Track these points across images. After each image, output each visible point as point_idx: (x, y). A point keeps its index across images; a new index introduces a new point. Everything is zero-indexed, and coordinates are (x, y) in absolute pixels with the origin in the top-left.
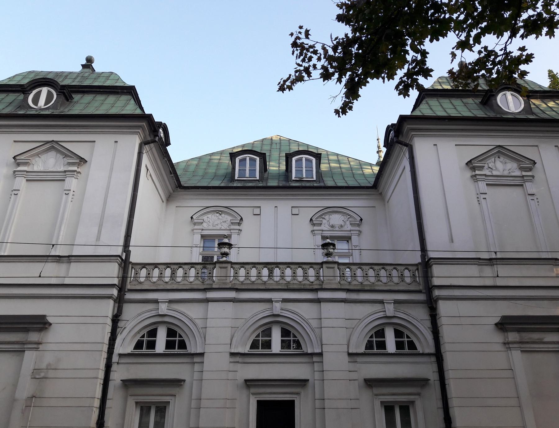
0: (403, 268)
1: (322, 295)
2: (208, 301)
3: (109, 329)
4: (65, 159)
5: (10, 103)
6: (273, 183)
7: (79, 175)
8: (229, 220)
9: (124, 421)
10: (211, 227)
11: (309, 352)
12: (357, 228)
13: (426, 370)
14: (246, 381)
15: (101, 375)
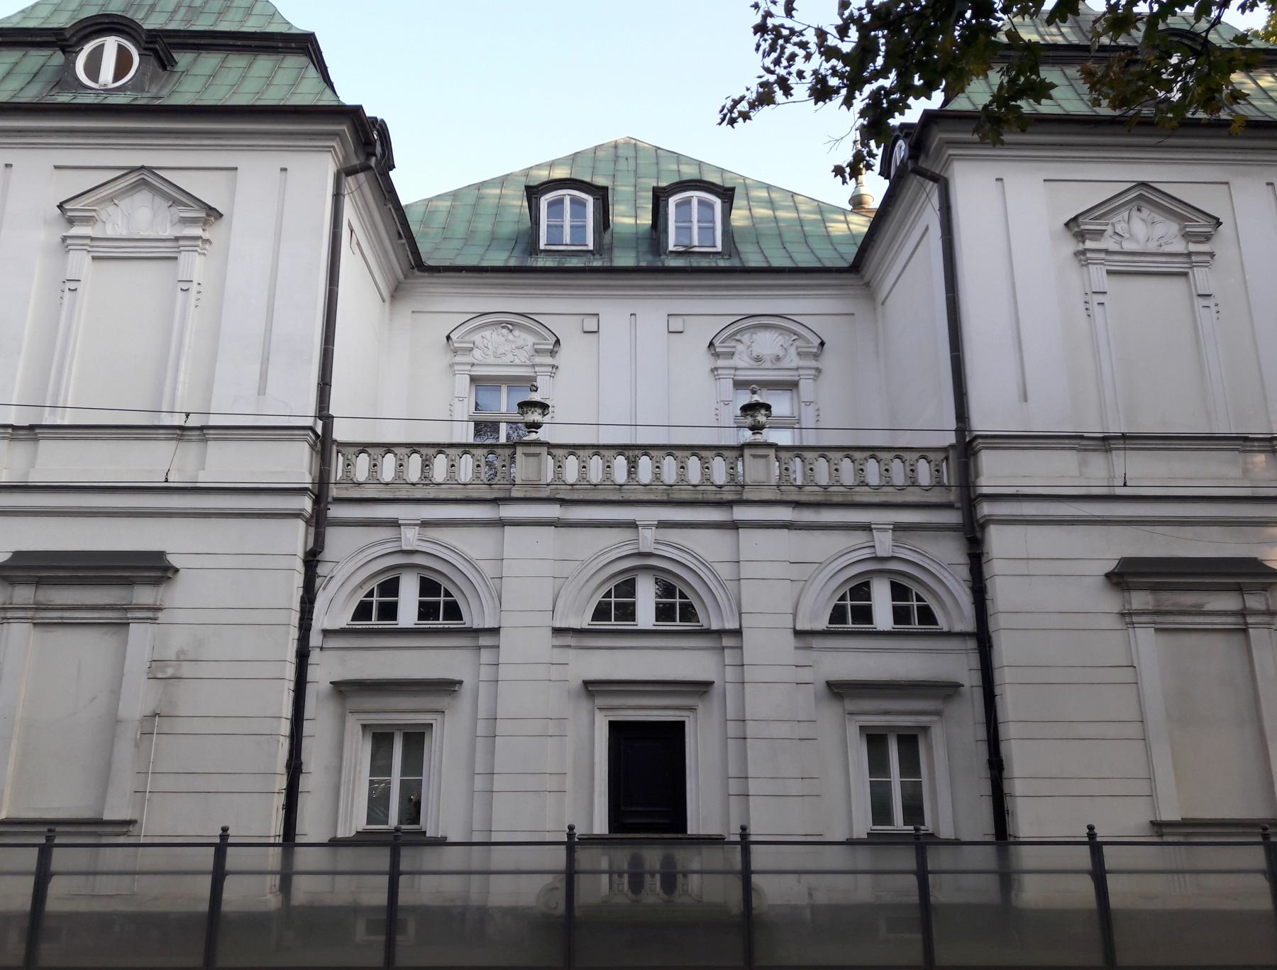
0: (915, 455)
1: (741, 513)
2: (502, 523)
3: (299, 579)
4: (173, 209)
5: (36, 75)
6: (625, 259)
7: (207, 246)
8: (530, 344)
9: (341, 758)
10: (491, 360)
11: (714, 627)
12: (813, 363)
13: (957, 665)
14: (587, 683)
15: (290, 672)
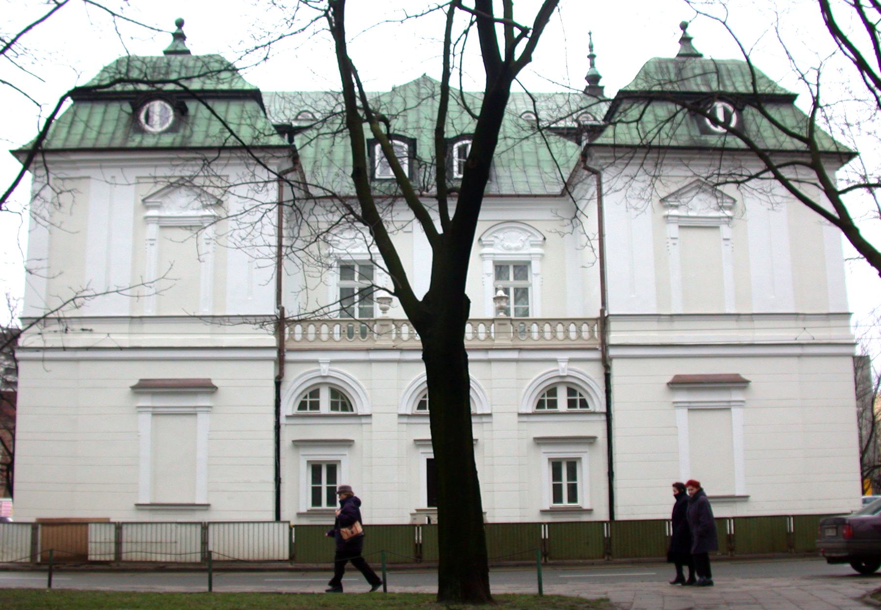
13: (597, 429)
